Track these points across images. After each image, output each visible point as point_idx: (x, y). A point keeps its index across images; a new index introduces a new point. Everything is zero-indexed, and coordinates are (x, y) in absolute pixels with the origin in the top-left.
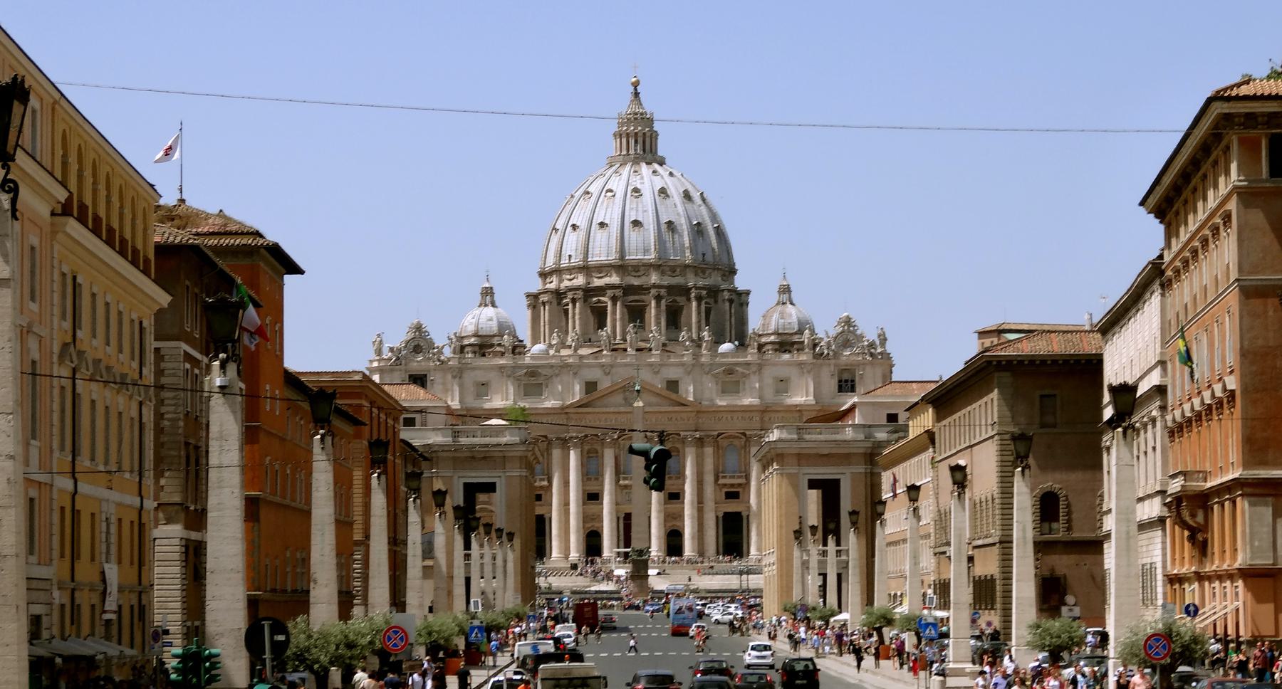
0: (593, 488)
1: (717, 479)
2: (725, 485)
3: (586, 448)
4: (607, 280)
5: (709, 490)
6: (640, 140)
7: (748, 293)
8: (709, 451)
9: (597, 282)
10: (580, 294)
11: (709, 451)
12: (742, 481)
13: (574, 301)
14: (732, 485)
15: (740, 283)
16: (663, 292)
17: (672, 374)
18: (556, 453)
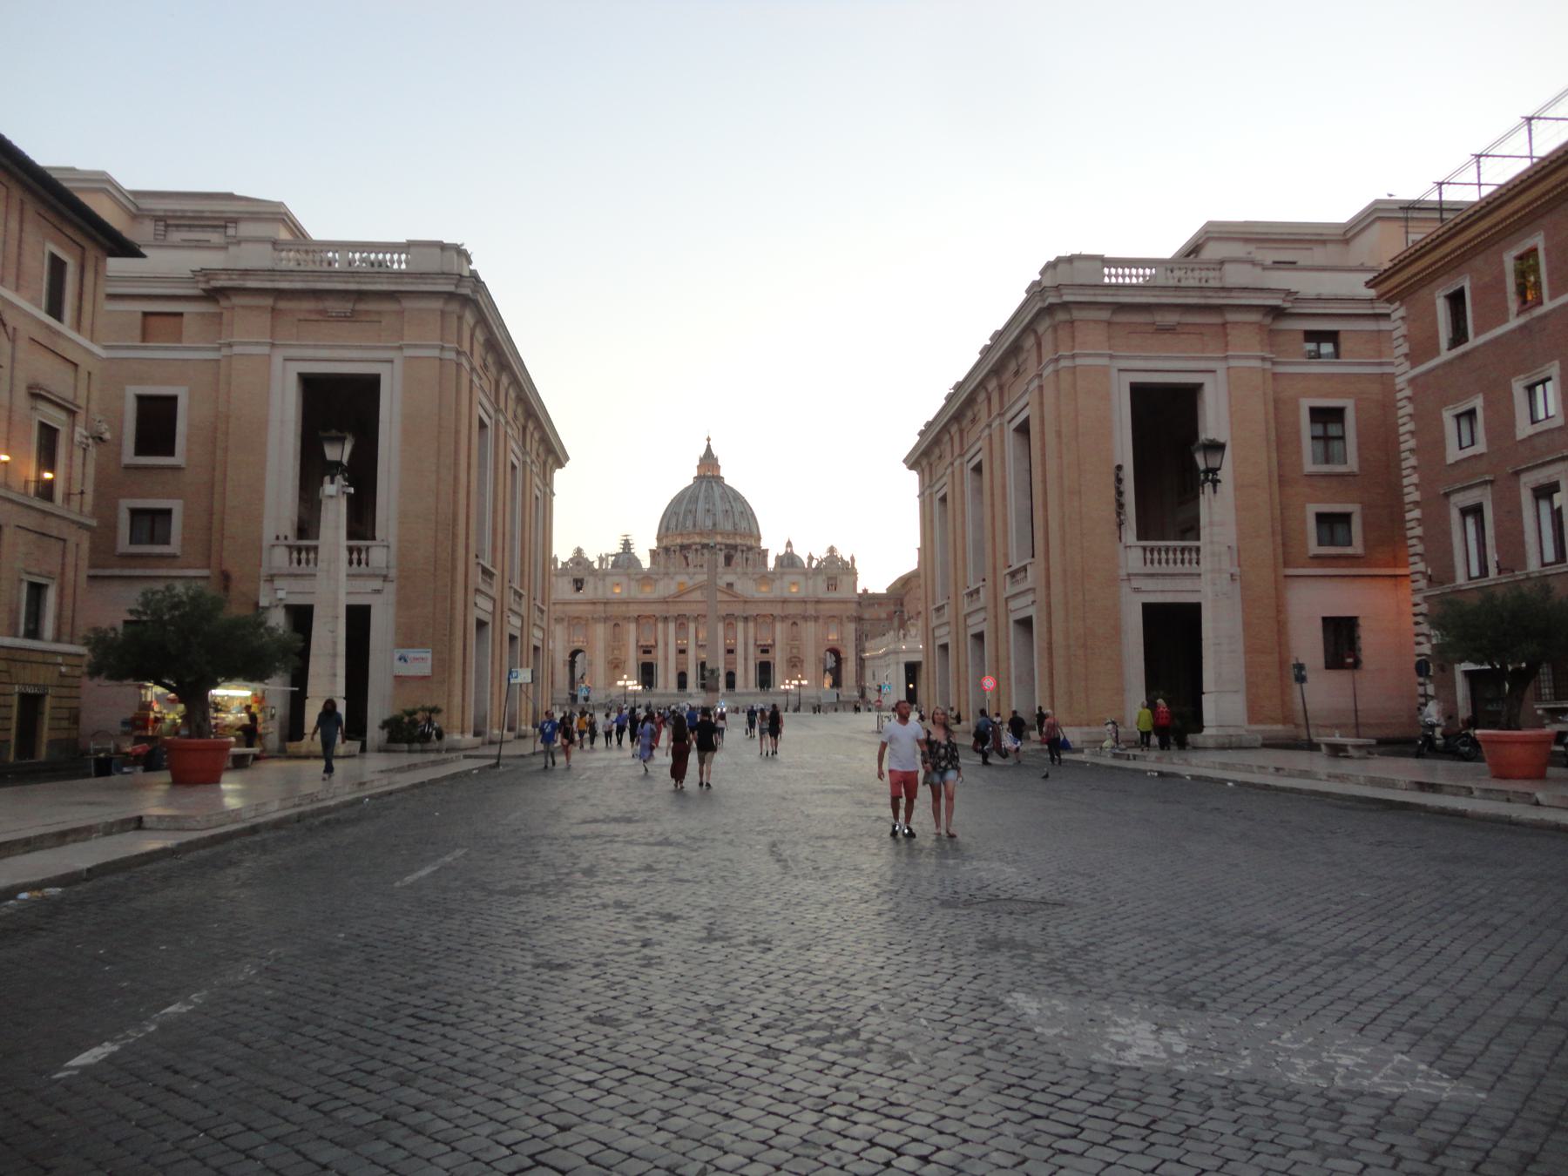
5: (751, 648)
8: (751, 624)
9: (686, 542)
11: (751, 624)
15: (764, 545)
17: (729, 578)
18: (660, 626)
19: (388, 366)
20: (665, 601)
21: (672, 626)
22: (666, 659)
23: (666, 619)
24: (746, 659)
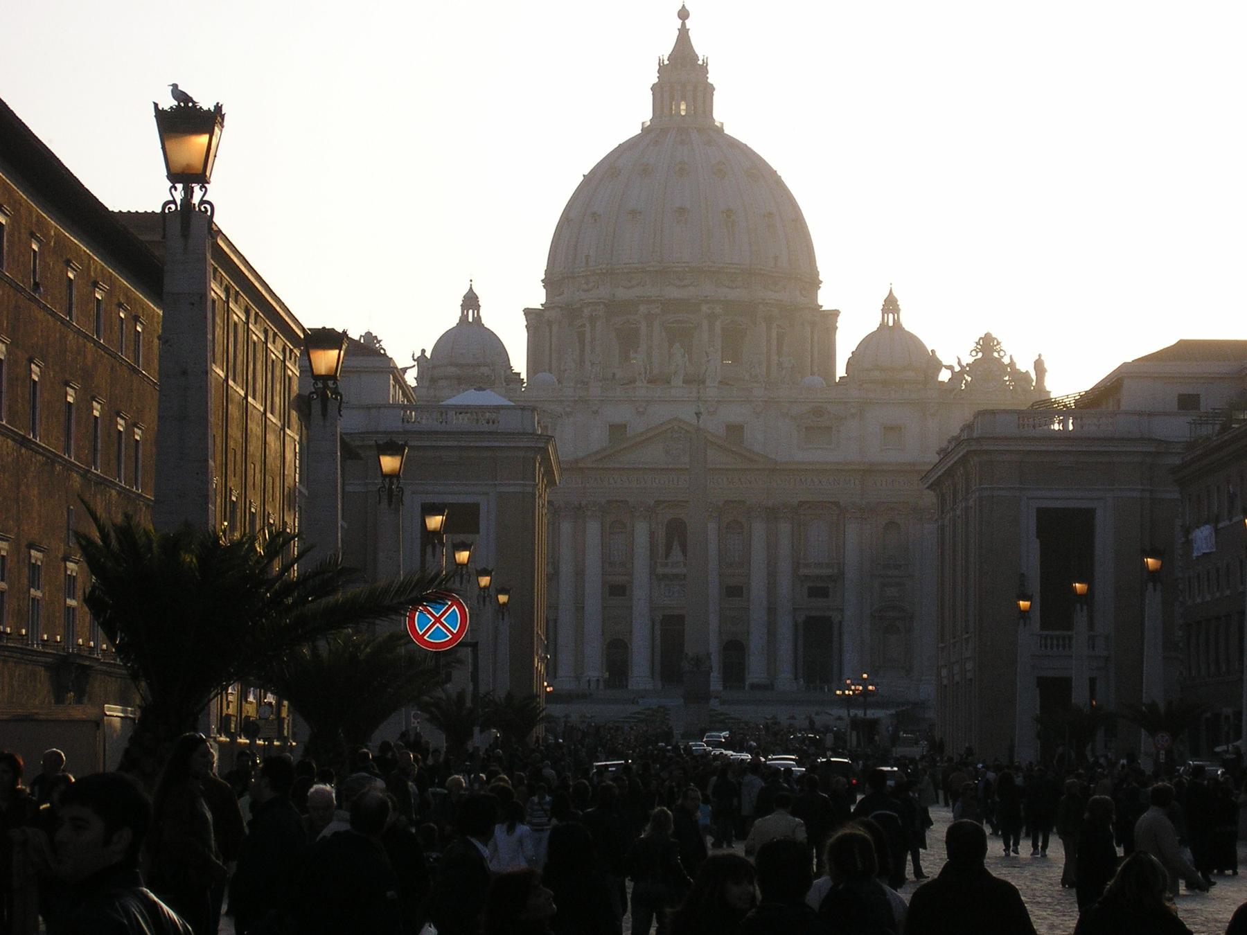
7: (835, 314)
9: (622, 294)
16: (718, 309)
21: (593, 529)
22: (580, 608)
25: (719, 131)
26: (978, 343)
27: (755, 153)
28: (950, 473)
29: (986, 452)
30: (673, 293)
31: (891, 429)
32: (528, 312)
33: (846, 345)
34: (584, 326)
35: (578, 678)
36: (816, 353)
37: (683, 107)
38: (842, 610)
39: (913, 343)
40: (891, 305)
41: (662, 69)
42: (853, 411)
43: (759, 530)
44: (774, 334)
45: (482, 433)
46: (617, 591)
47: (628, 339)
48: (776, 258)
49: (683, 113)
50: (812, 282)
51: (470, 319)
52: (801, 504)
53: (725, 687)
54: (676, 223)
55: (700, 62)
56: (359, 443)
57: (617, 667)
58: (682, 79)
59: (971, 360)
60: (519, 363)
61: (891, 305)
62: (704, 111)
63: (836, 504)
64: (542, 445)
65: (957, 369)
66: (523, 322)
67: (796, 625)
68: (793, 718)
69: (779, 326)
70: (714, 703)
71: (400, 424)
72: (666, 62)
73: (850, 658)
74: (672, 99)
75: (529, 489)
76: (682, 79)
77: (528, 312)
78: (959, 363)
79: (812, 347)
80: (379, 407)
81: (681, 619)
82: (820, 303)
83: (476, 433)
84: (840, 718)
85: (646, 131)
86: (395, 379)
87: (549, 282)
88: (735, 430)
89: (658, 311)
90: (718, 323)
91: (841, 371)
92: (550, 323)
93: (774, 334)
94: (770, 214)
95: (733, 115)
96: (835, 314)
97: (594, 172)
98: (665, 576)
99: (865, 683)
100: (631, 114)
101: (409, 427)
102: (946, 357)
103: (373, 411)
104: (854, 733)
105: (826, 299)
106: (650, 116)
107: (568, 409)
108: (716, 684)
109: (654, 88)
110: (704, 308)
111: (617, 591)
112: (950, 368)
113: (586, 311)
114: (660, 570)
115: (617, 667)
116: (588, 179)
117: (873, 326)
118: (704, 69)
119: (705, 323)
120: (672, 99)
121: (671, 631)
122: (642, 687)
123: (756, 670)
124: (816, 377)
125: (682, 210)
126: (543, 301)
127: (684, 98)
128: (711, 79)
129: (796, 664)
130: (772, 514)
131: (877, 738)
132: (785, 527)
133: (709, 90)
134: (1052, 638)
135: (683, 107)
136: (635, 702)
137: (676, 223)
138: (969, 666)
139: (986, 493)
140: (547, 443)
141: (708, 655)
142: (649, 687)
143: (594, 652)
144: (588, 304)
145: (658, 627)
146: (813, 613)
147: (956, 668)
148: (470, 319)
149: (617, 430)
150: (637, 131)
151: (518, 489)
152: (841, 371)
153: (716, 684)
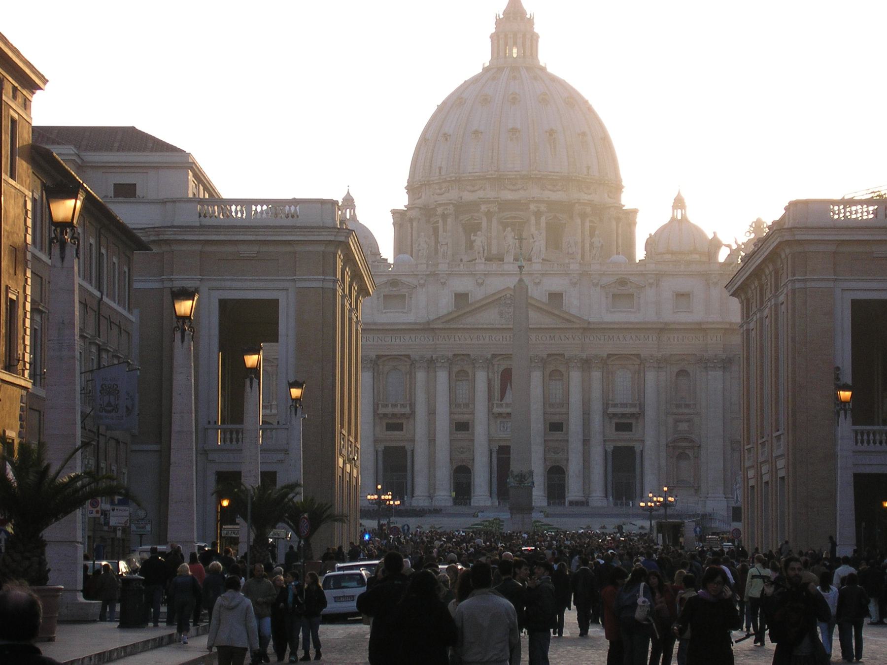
0: (460, 435)
1: (606, 405)
2: (615, 415)
3: (456, 369)
4: (481, 194)
6: (520, 41)
7: (634, 212)
9: (468, 197)
10: (451, 209)
12: (407, 410)
13: (444, 217)
14: (624, 415)
16: (543, 208)
18: (420, 376)
19: (285, 292)
20: (427, 328)
21: (442, 377)
22: (432, 441)
23: (431, 364)
24: (586, 442)
25: (543, 69)
26: (751, 226)
27: (569, 85)
28: (757, 273)
29: (799, 242)
30: (508, 195)
31: (682, 296)
32: (395, 212)
33: (643, 232)
34: (437, 222)
35: (431, 497)
36: (620, 232)
37: (515, 51)
38: (643, 441)
39: (697, 232)
40: (679, 203)
41: (498, 22)
42: (651, 281)
43: (575, 377)
44: (587, 228)
45: (281, 227)
46: (462, 426)
47: (472, 228)
48: (588, 168)
49: (515, 55)
50: (617, 188)
51: (348, 217)
52: (609, 356)
53: (549, 504)
54: (508, 144)
55: (528, 16)
56: (152, 238)
57: (462, 488)
58: (514, 32)
59: (745, 240)
60: (387, 250)
61: (679, 203)
62: (531, 55)
63: (638, 356)
64: (342, 239)
65: (734, 247)
66: (390, 215)
67: (606, 452)
68: (604, 527)
69: (591, 221)
70: (536, 516)
71: (197, 219)
72: (501, 16)
73: (650, 478)
74: (506, 44)
75: (331, 285)
76: (514, 32)
77: (395, 212)
78: (736, 243)
79: (617, 236)
80: (174, 201)
81: (508, 448)
82: (623, 202)
83: (276, 227)
84: (642, 528)
85: (486, 70)
86: (196, 176)
87: (412, 189)
88: (556, 297)
89: (496, 209)
90: (543, 219)
91: (640, 254)
92: (411, 220)
93: (587, 228)
94: (584, 134)
95: (553, 57)
96: (634, 212)
97: (444, 103)
98: (500, 414)
99: (665, 495)
100: (476, 58)
101: (207, 221)
102: (724, 239)
103: (169, 206)
104: (660, 535)
105: (627, 201)
106: (489, 58)
107: (422, 282)
108: (539, 495)
109: (492, 37)
110: (532, 207)
111: (462, 426)
112: (729, 246)
113: (440, 210)
114: (496, 410)
115: (462, 488)
116: (441, 109)
117: (665, 219)
118: (531, 21)
119: (533, 219)
120: (506, 44)
121: (502, 456)
122: (482, 504)
123: (574, 491)
124: (621, 256)
125: (514, 130)
126: (406, 203)
127: (515, 44)
128: (537, 29)
129: (606, 487)
130: (586, 364)
131: (681, 540)
132: (596, 375)
133: (534, 38)
134: (862, 434)
135: (515, 51)
136: (475, 516)
137: (508, 144)
138: (781, 463)
139: (798, 285)
140: (347, 237)
141: (531, 473)
142: (488, 503)
143: (444, 474)
144: (440, 205)
145: (494, 455)
146: (620, 444)
147: (765, 469)
148: (348, 217)
149: (461, 298)
150: (479, 70)
151: (320, 284)
152: (640, 254)
153: (539, 495)
